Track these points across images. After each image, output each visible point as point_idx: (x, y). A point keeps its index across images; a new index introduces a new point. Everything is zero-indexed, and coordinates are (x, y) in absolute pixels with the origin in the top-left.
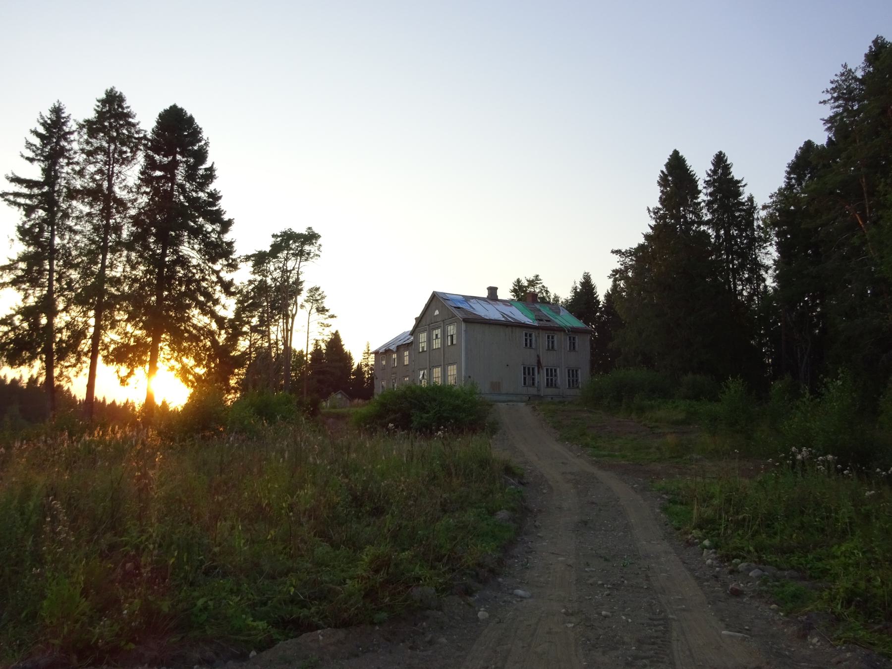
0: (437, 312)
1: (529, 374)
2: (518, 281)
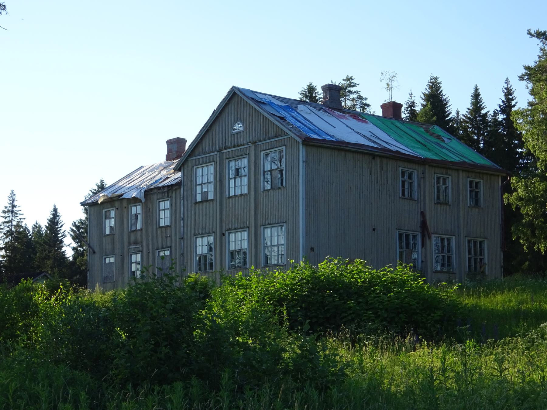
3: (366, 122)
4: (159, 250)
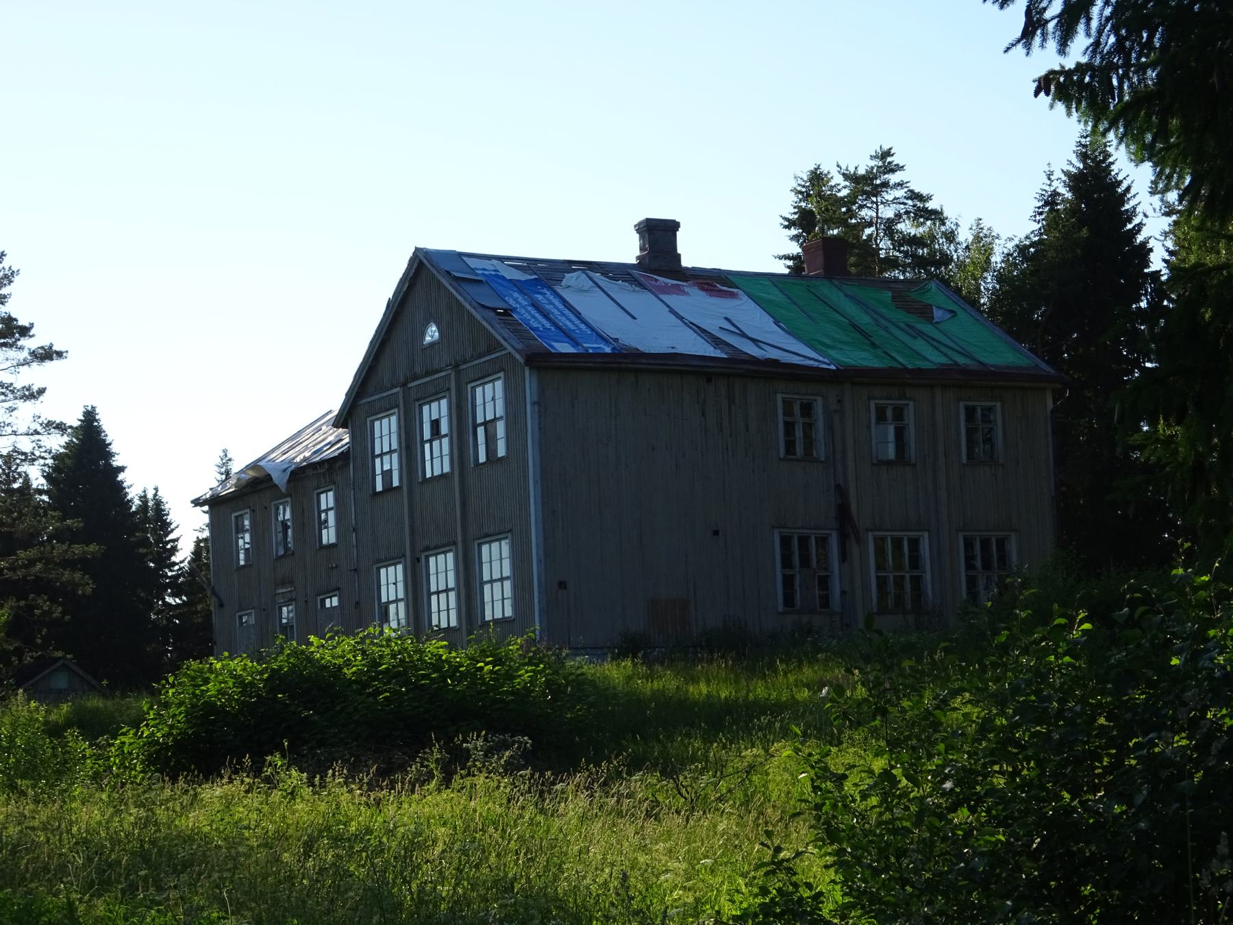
0: (432, 333)
1: (805, 561)
2: (817, 178)
3: (733, 295)
4: (322, 597)
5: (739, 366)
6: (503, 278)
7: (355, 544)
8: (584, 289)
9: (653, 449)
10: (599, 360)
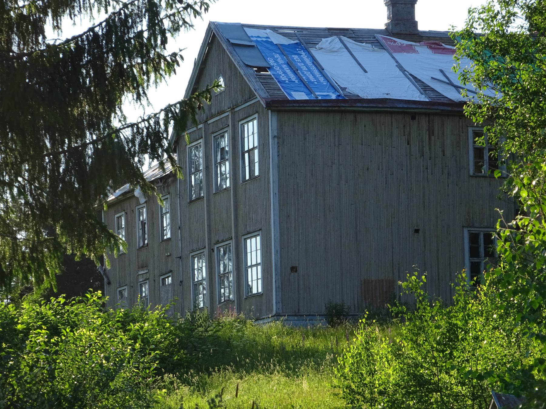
4: (163, 277)
5: (436, 107)
6: (271, 43)
7: (180, 238)
8: (335, 50)
9: (368, 169)
10: (323, 105)
